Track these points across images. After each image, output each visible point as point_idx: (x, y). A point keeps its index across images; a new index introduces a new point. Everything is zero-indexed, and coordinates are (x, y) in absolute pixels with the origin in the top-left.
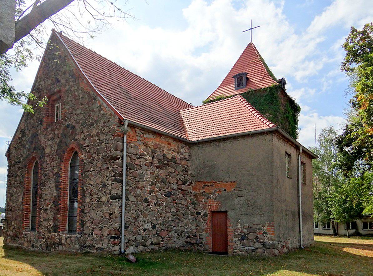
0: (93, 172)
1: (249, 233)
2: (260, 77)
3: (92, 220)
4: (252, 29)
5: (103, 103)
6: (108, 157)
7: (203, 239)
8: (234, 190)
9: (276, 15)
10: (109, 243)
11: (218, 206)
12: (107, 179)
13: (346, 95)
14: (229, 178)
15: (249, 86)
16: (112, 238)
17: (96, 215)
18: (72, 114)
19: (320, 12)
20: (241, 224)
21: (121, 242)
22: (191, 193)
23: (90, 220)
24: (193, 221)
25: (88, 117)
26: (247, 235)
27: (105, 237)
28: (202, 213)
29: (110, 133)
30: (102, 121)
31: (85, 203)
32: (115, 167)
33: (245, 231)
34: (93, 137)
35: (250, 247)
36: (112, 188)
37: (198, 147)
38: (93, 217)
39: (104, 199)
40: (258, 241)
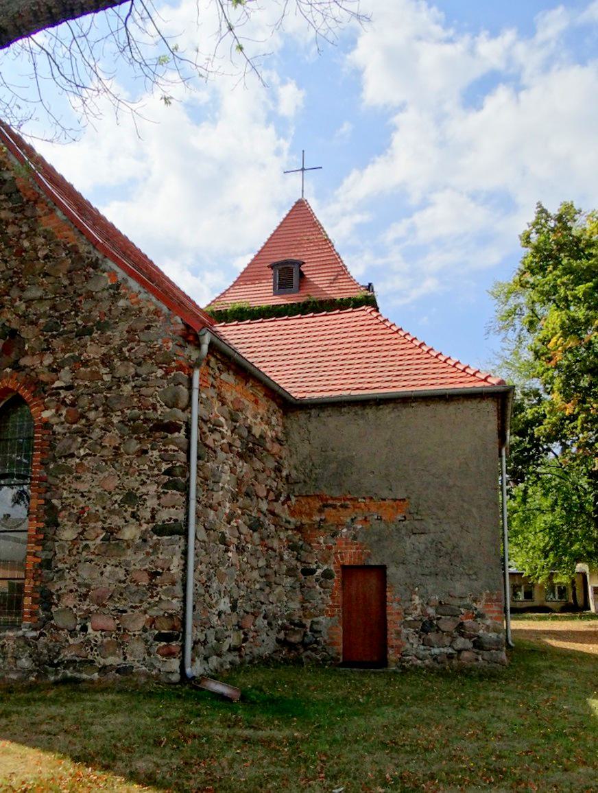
0: (89, 458)
1: (439, 616)
2: (330, 274)
3: (84, 590)
4: (305, 171)
5: (125, 280)
6: (144, 423)
7: (320, 632)
8: (403, 519)
9: (278, 152)
10: (149, 654)
11: (362, 553)
12: (142, 480)
13: (488, 333)
14: (391, 490)
15: (305, 291)
16: (159, 638)
17: (106, 577)
18: (7, 298)
19: (363, 165)
20: (421, 597)
21: (183, 648)
22: (289, 522)
23: (77, 591)
24: (295, 588)
25: (71, 311)
26: (435, 622)
27: (134, 635)
28: (319, 571)
29: (151, 359)
30: (123, 326)
31: (57, 544)
32: (171, 450)
33: (431, 611)
34: (87, 366)
35: (443, 647)
36: (159, 505)
37: (306, 413)
38: (86, 581)
39: (130, 533)
40: (462, 635)
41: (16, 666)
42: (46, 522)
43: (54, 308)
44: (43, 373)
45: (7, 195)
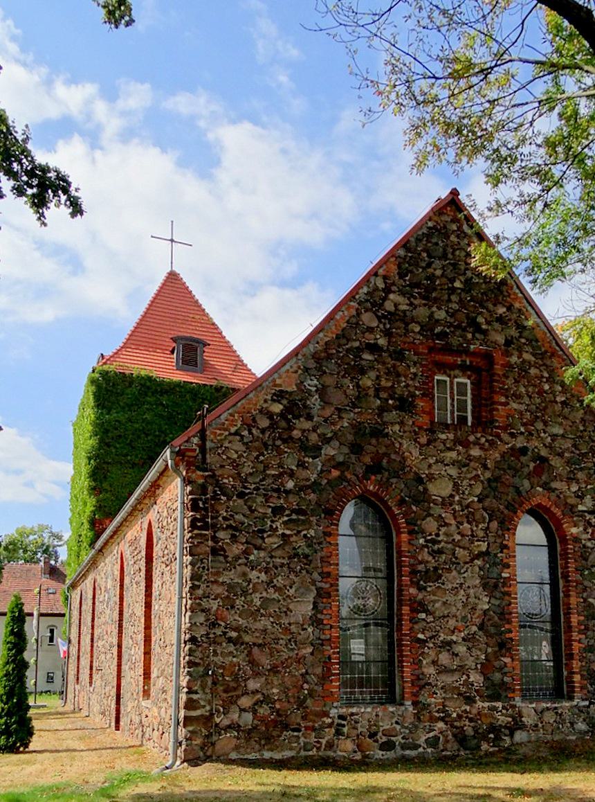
41: (574, 729)
42: (586, 616)
43: (575, 446)
44: (571, 497)
45: (527, 340)
